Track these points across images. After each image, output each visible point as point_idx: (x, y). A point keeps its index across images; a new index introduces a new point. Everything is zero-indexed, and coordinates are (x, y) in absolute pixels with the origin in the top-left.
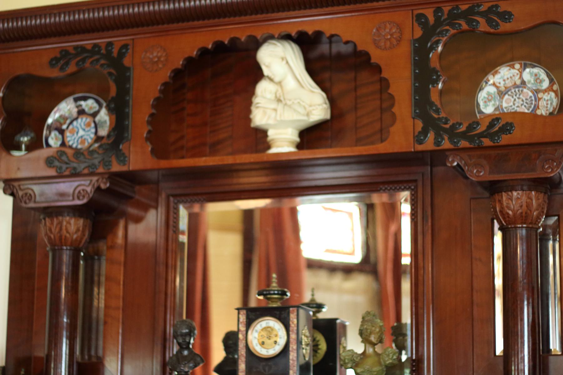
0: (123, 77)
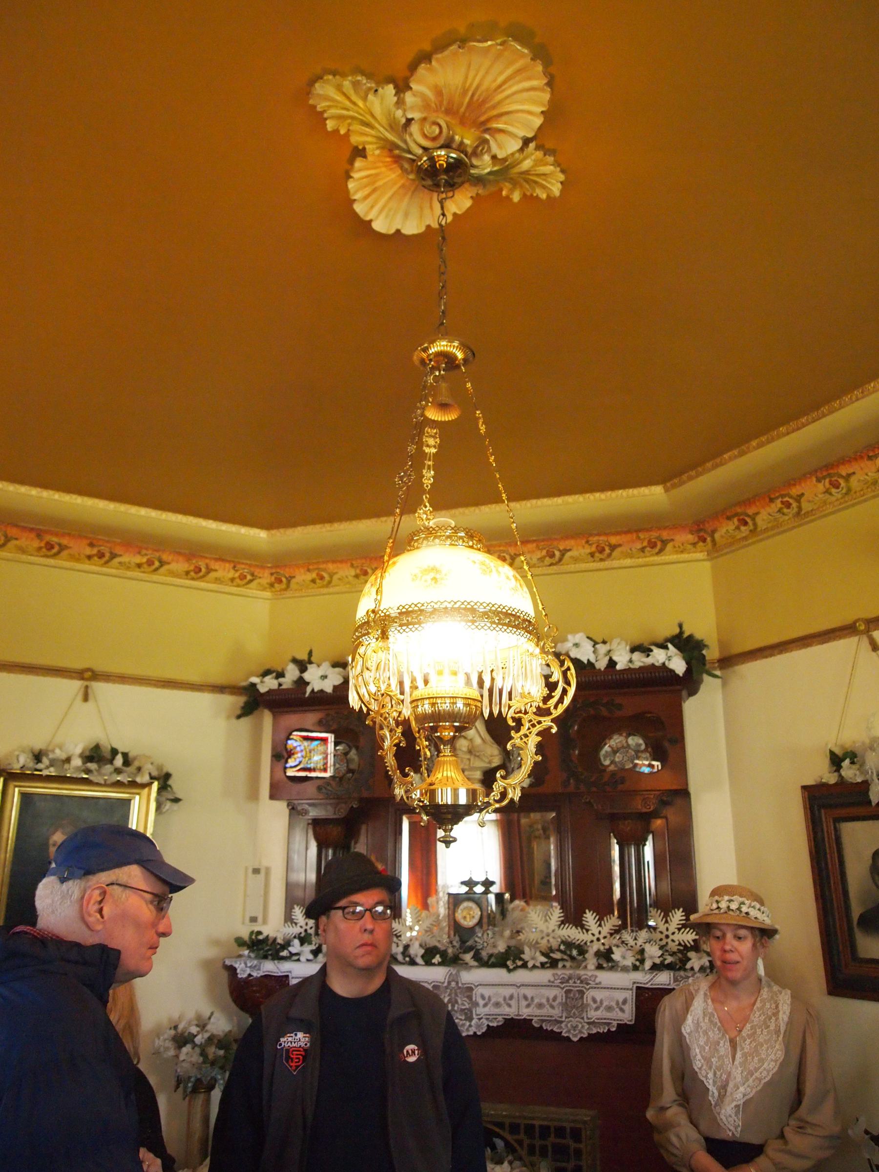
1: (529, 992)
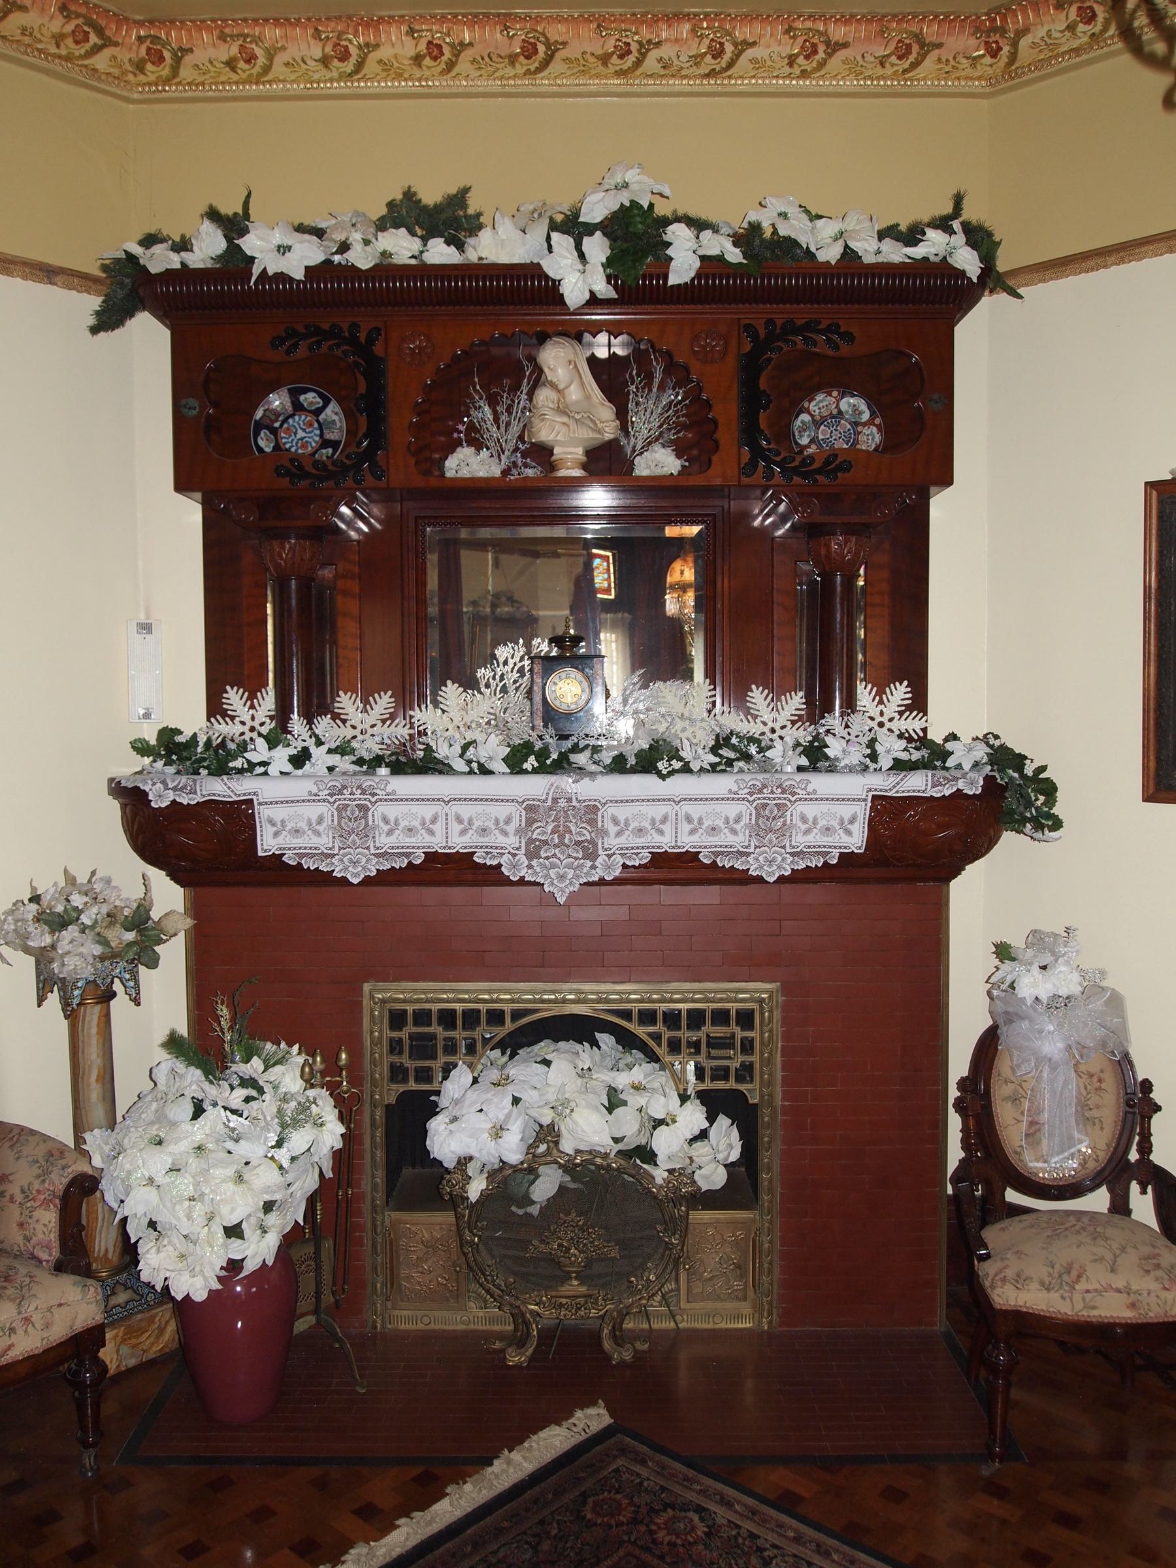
0: (374, 369)
1: (695, 810)
